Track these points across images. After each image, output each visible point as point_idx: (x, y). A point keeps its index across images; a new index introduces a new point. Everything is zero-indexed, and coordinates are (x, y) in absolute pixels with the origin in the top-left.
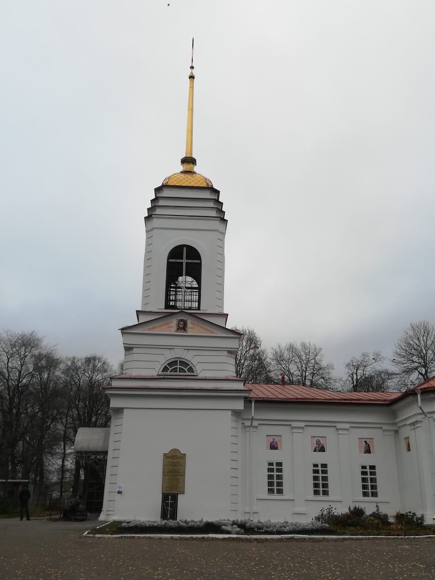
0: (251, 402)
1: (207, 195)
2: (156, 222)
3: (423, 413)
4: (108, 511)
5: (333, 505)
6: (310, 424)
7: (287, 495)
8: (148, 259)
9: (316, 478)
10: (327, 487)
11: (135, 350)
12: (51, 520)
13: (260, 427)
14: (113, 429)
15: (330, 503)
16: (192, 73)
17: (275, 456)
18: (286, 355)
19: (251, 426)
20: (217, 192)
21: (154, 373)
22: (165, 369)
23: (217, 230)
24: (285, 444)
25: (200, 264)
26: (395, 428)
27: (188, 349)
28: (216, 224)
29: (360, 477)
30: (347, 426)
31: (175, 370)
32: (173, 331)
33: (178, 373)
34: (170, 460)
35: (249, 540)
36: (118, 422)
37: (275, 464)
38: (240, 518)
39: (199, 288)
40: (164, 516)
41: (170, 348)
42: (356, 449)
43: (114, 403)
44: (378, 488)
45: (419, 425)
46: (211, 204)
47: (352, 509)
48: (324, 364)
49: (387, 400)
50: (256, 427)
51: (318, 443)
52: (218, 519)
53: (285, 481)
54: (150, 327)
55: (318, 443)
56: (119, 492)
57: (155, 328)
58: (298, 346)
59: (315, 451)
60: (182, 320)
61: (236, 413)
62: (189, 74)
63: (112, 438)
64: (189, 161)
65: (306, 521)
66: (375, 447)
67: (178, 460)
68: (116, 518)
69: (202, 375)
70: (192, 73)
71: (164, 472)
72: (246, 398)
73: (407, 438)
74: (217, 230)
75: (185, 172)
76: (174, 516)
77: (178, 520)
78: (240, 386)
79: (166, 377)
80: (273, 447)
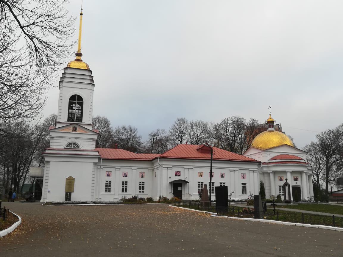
0: (101, 159)
1: (86, 73)
2: (64, 84)
3: (160, 165)
4: (44, 199)
5: (126, 195)
6: (122, 167)
7: (112, 192)
8: (60, 100)
9: (123, 186)
10: (140, 186)
11: (55, 138)
12: (21, 202)
13: (104, 168)
14: (45, 169)
15: (125, 195)
16: (81, 12)
17: (108, 179)
18: (122, 131)
19: (100, 168)
20: (91, 71)
21: (62, 148)
22: (67, 146)
23: (90, 89)
24: (113, 175)
25: (83, 103)
26: (153, 169)
27: (77, 138)
28: (90, 87)
29: (139, 186)
30: (136, 168)
31: (71, 147)
32: (71, 131)
33: (72, 148)
34: (68, 180)
35: (96, 206)
36: (48, 166)
37: (76, 103)
38: (94, 200)
39: (82, 110)
40: (66, 199)
41: (70, 138)
42: (139, 176)
43: (46, 159)
44: (111, 187)
45: (158, 169)
46: (88, 78)
47: (133, 196)
48: (138, 135)
49: (151, 159)
50: (102, 168)
51: (125, 174)
52: (86, 201)
53: (112, 188)
54: (62, 129)
55: (125, 174)
56: (49, 192)
57: (63, 130)
58: (127, 127)
59: (123, 177)
60: (75, 127)
61: (95, 164)
62: (80, 13)
63: (45, 172)
64: (79, 54)
65: (116, 201)
66: (145, 176)
67: (72, 180)
68: (48, 201)
69: (82, 149)
70: (81, 12)
71: (66, 185)
72: (99, 158)
73: (156, 173)
74: (90, 89)
75: (76, 60)
76: (70, 199)
77: (71, 201)
78: (97, 153)
79: (68, 149)
80: (108, 175)
